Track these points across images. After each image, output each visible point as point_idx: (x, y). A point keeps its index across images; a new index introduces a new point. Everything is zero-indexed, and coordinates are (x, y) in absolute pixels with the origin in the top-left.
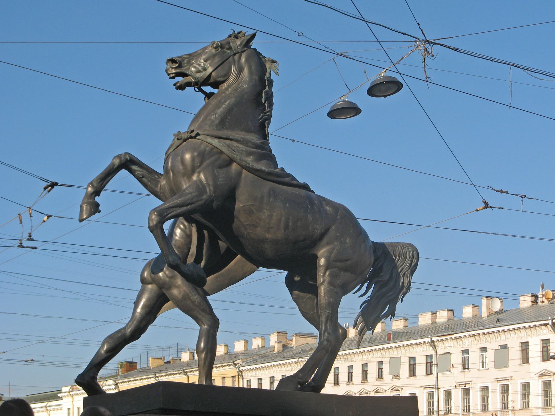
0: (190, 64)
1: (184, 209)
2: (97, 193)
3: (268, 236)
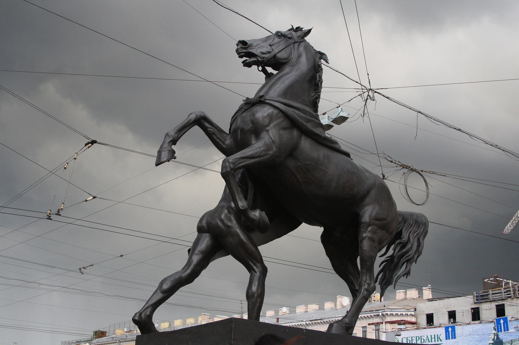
1: (254, 160)
2: (174, 142)
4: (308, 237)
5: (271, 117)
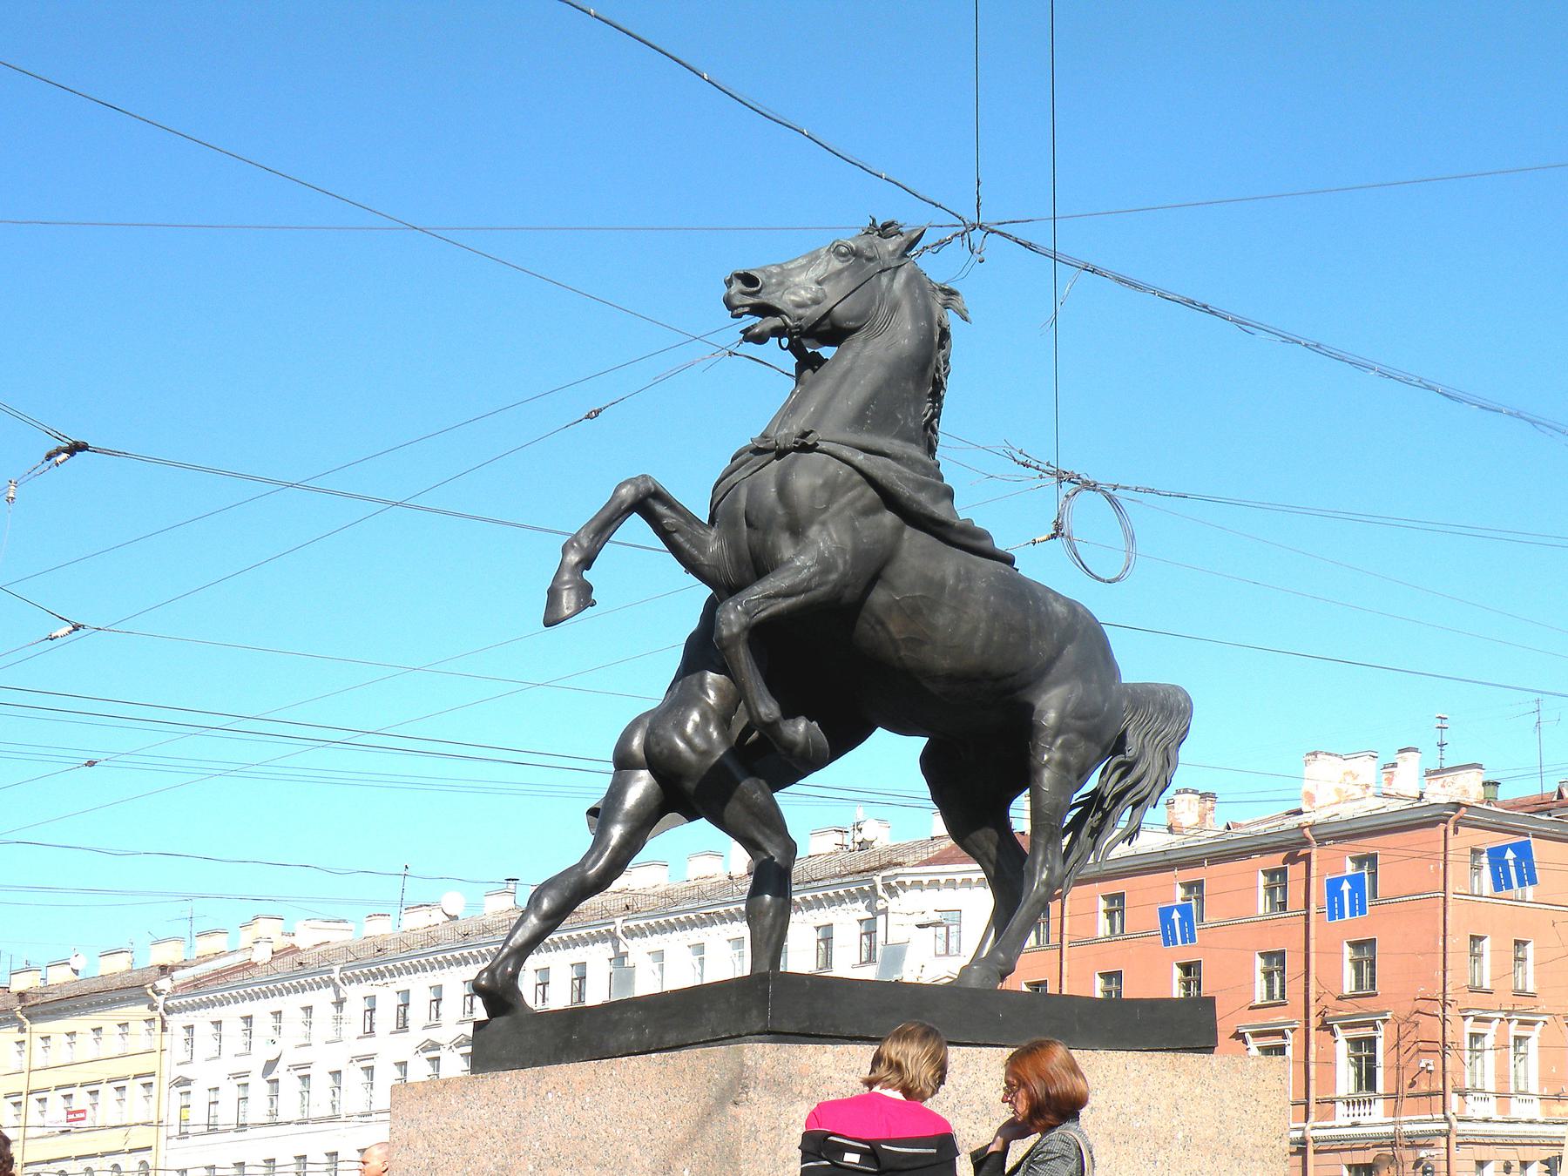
1: (793, 600)
2: (587, 562)
4: (890, 761)
5: (833, 488)
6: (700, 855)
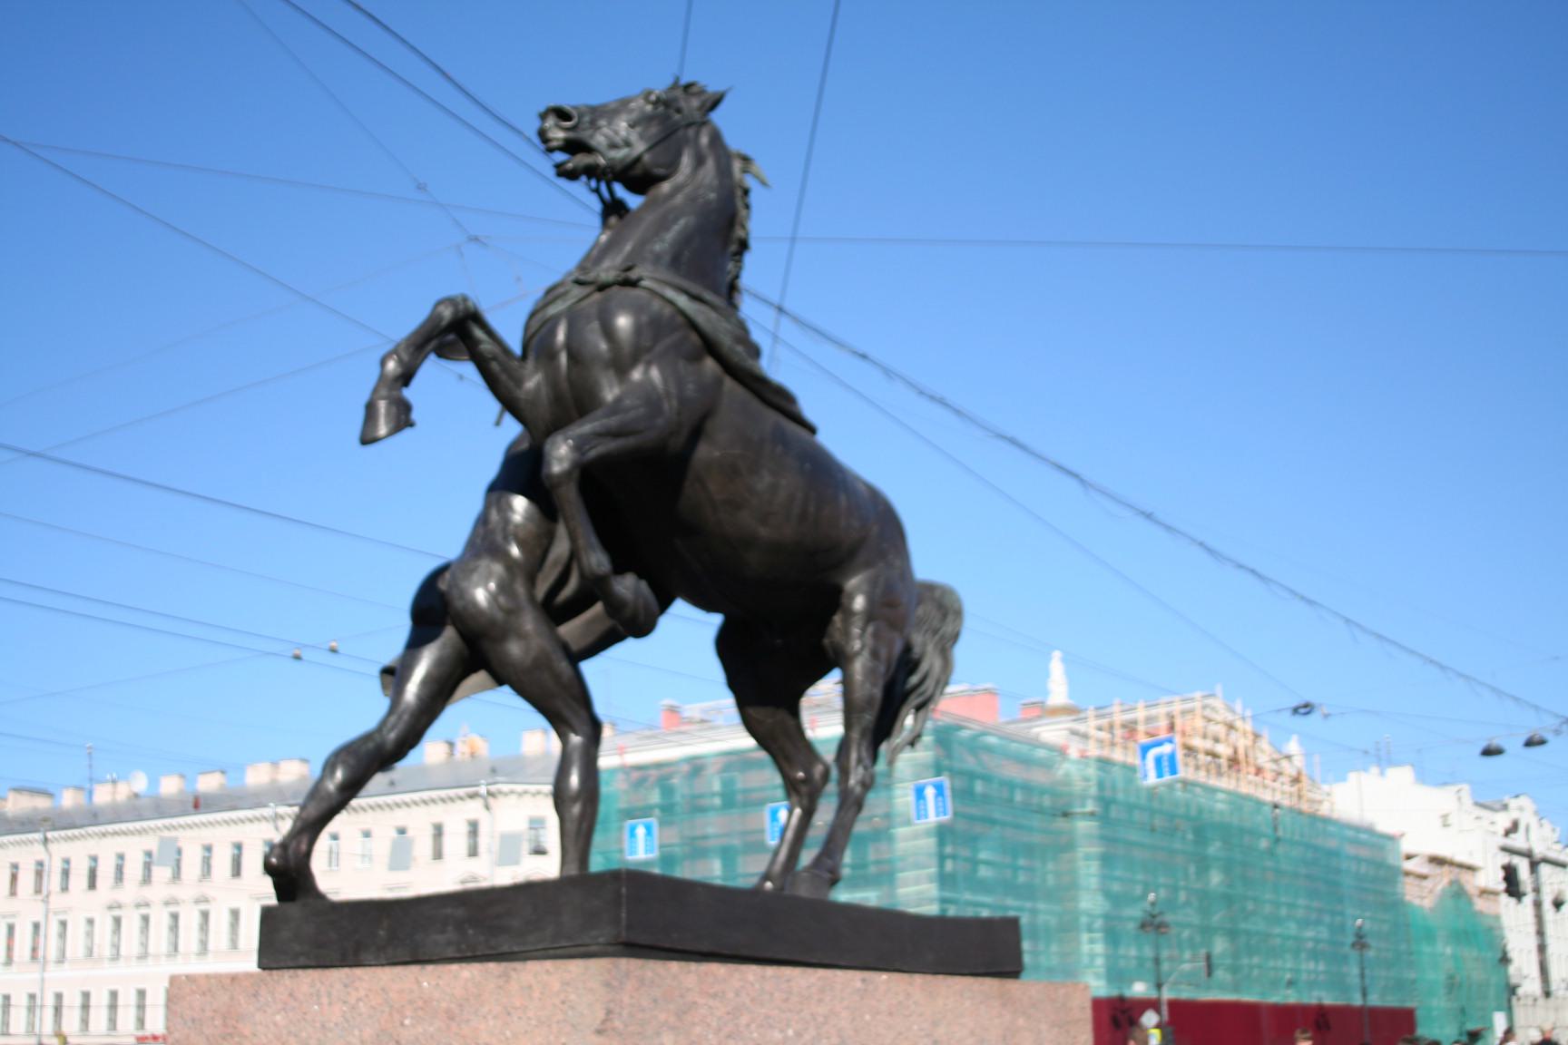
0: (594, 125)
2: (406, 377)
3: (763, 532)
4: (689, 632)
6: (494, 726)
